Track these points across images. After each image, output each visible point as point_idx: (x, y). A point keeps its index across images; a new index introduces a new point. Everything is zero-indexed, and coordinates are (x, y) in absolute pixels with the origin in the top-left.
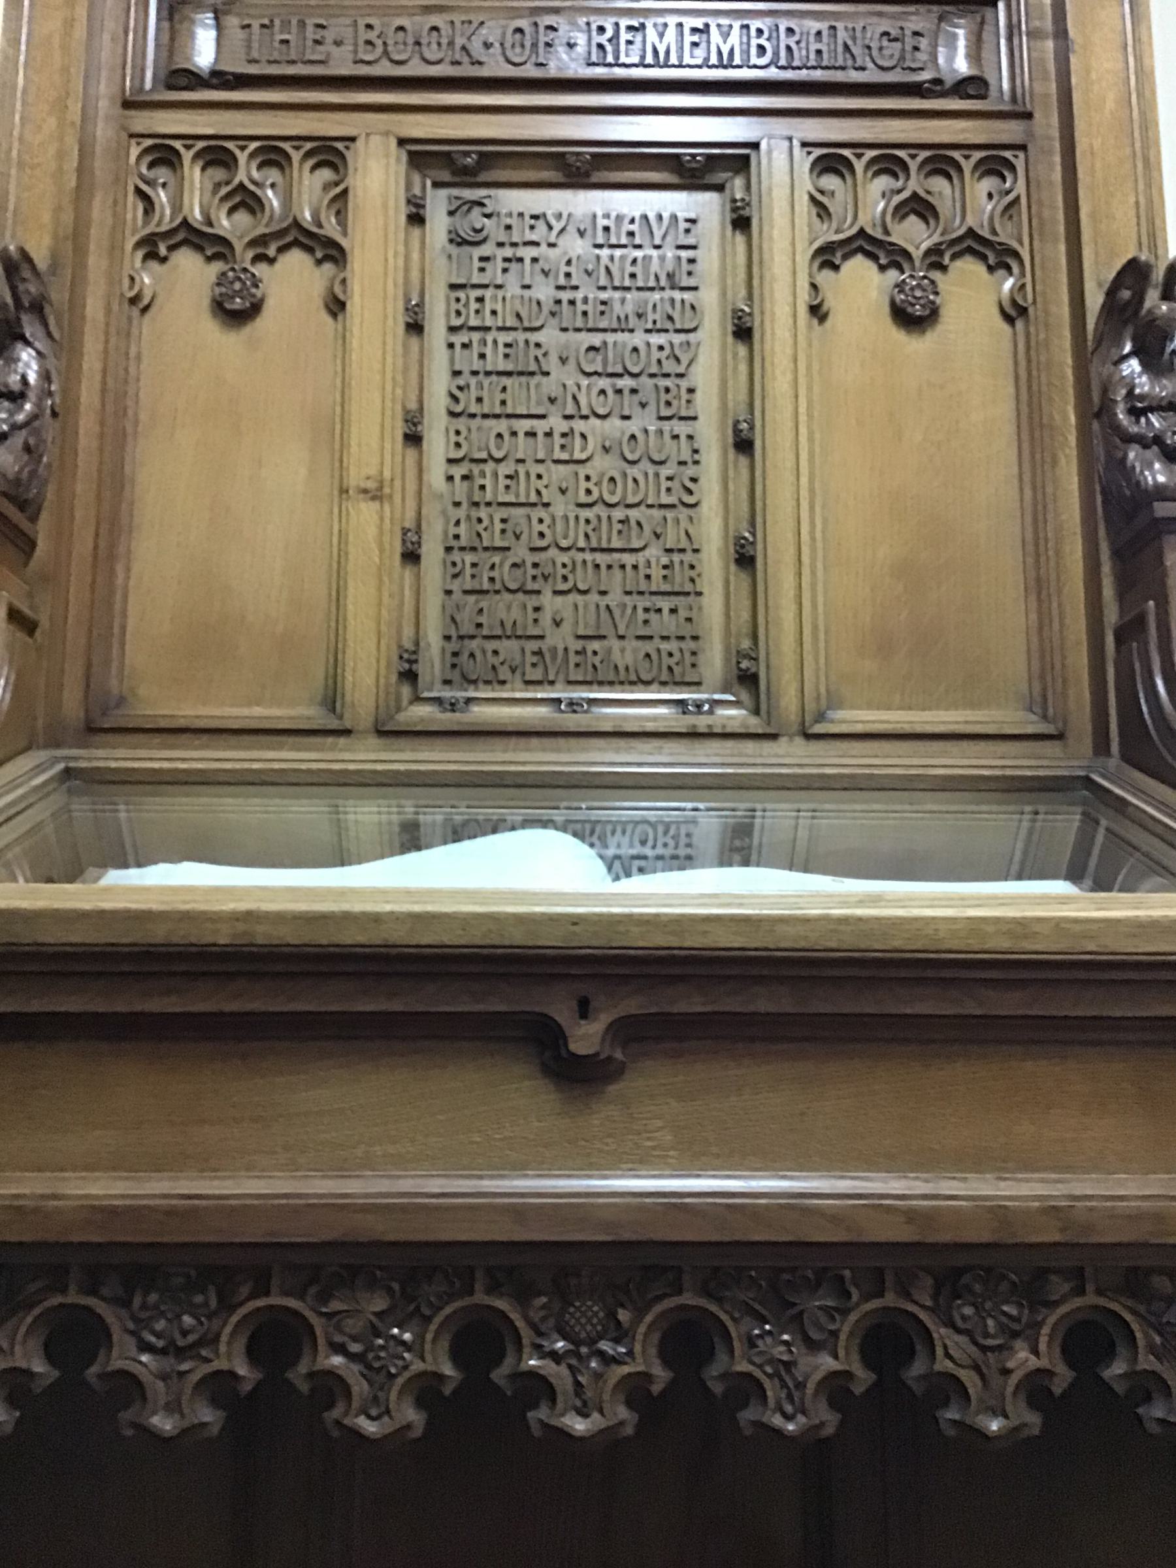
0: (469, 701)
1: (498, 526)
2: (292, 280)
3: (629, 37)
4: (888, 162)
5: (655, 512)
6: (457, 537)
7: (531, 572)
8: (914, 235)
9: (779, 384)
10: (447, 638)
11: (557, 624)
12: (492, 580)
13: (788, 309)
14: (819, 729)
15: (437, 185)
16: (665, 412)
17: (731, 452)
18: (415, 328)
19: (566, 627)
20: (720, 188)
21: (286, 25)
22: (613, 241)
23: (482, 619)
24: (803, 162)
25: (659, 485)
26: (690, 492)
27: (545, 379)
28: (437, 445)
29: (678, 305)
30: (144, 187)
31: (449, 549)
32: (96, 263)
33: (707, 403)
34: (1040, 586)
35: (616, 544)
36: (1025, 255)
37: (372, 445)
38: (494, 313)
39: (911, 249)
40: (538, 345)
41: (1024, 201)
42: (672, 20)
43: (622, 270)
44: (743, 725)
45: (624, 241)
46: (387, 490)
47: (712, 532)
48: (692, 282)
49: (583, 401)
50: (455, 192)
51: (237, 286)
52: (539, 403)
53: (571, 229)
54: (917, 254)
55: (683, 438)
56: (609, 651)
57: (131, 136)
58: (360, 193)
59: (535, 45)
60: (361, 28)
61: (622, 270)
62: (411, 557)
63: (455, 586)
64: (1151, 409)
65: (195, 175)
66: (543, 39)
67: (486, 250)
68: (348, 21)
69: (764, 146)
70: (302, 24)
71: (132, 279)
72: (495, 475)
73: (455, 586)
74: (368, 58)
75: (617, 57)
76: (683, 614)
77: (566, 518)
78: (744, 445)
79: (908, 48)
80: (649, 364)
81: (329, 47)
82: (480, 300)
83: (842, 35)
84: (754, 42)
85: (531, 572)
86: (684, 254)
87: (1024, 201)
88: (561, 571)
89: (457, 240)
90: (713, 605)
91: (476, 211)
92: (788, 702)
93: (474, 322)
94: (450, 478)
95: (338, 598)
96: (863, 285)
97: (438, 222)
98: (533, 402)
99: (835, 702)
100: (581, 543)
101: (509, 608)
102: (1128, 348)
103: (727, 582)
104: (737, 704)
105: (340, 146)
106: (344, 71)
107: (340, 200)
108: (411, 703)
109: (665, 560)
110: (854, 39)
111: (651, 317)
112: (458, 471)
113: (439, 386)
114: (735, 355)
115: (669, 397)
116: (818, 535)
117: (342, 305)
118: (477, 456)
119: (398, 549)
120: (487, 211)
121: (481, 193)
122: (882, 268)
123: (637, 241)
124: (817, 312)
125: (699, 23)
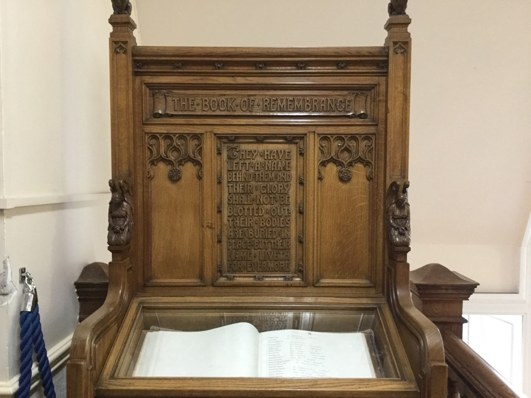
0: (234, 276)
1: (241, 233)
2: (188, 170)
3: (273, 103)
4: (340, 137)
5: (279, 229)
6: (230, 235)
7: (249, 244)
8: (345, 157)
9: (310, 198)
10: (229, 261)
11: (255, 257)
12: (239, 246)
13: (313, 178)
14: (317, 285)
15: (224, 143)
16: (282, 203)
17: (298, 214)
18: (220, 183)
19: (257, 257)
20: (297, 143)
21: (184, 99)
22: (269, 158)
23: (237, 256)
24: (317, 139)
25: (280, 222)
26: (288, 223)
27: (252, 195)
28: (225, 212)
29: (285, 175)
30: (150, 147)
31: (228, 239)
32: (139, 168)
33: (292, 200)
34: (372, 250)
35: (269, 237)
36: (373, 163)
37: (209, 209)
38: (239, 177)
39: (344, 162)
40: (250, 186)
41: (374, 149)
42: (285, 98)
43: (271, 166)
44: (300, 283)
45: (272, 158)
46: (213, 226)
47: (293, 234)
48: (289, 169)
49: (261, 201)
50: (229, 145)
51: (175, 173)
52: (251, 201)
53: (258, 154)
54: (346, 164)
55: (286, 210)
56: (267, 263)
57: (146, 133)
58: (205, 149)
59: (249, 105)
60: (204, 101)
61: (271, 166)
62: (220, 241)
63: (230, 247)
64: (398, 219)
65: (163, 143)
66: (251, 104)
67: (237, 161)
68: (200, 98)
69: (308, 134)
70: (188, 99)
71: (149, 172)
72: (240, 220)
73: (230, 247)
74: (205, 110)
75: (270, 108)
76: (285, 254)
77: (257, 231)
78: (301, 213)
79: (347, 105)
80: (278, 190)
81: (195, 106)
82: (235, 174)
83: (329, 102)
84: (306, 104)
85: (249, 244)
86: (287, 162)
87: (374, 149)
88: (256, 244)
89: (229, 158)
90: (293, 252)
91: (234, 150)
92: (310, 278)
93: (234, 180)
94: (229, 221)
95: (202, 253)
96: (332, 170)
97: (225, 154)
98: (249, 201)
99: (321, 277)
100: (261, 237)
101: (243, 253)
102: (394, 201)
103: (296, 247)
104: (298, 277)
105: (199, 135)
106: (199, 113)
107: (200, 151)
108: (220, 277)
109: (281, 241)
110: (332, 102)
111: (278, 178)
112: (230, 219)
113: (226, 196)
114: (300, 188)
115: (283, 199)
116: (319, 236)
117: (201, 178)
118: (235, 215)
119: (216, 240)
120: (238, 150)
121: (236, 145)
122: (337, 166)
123: (275, 158)
124: (320, 179)
125: (291, 98)
